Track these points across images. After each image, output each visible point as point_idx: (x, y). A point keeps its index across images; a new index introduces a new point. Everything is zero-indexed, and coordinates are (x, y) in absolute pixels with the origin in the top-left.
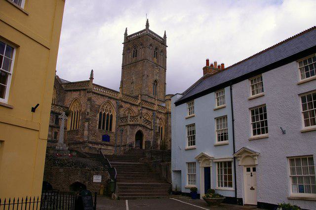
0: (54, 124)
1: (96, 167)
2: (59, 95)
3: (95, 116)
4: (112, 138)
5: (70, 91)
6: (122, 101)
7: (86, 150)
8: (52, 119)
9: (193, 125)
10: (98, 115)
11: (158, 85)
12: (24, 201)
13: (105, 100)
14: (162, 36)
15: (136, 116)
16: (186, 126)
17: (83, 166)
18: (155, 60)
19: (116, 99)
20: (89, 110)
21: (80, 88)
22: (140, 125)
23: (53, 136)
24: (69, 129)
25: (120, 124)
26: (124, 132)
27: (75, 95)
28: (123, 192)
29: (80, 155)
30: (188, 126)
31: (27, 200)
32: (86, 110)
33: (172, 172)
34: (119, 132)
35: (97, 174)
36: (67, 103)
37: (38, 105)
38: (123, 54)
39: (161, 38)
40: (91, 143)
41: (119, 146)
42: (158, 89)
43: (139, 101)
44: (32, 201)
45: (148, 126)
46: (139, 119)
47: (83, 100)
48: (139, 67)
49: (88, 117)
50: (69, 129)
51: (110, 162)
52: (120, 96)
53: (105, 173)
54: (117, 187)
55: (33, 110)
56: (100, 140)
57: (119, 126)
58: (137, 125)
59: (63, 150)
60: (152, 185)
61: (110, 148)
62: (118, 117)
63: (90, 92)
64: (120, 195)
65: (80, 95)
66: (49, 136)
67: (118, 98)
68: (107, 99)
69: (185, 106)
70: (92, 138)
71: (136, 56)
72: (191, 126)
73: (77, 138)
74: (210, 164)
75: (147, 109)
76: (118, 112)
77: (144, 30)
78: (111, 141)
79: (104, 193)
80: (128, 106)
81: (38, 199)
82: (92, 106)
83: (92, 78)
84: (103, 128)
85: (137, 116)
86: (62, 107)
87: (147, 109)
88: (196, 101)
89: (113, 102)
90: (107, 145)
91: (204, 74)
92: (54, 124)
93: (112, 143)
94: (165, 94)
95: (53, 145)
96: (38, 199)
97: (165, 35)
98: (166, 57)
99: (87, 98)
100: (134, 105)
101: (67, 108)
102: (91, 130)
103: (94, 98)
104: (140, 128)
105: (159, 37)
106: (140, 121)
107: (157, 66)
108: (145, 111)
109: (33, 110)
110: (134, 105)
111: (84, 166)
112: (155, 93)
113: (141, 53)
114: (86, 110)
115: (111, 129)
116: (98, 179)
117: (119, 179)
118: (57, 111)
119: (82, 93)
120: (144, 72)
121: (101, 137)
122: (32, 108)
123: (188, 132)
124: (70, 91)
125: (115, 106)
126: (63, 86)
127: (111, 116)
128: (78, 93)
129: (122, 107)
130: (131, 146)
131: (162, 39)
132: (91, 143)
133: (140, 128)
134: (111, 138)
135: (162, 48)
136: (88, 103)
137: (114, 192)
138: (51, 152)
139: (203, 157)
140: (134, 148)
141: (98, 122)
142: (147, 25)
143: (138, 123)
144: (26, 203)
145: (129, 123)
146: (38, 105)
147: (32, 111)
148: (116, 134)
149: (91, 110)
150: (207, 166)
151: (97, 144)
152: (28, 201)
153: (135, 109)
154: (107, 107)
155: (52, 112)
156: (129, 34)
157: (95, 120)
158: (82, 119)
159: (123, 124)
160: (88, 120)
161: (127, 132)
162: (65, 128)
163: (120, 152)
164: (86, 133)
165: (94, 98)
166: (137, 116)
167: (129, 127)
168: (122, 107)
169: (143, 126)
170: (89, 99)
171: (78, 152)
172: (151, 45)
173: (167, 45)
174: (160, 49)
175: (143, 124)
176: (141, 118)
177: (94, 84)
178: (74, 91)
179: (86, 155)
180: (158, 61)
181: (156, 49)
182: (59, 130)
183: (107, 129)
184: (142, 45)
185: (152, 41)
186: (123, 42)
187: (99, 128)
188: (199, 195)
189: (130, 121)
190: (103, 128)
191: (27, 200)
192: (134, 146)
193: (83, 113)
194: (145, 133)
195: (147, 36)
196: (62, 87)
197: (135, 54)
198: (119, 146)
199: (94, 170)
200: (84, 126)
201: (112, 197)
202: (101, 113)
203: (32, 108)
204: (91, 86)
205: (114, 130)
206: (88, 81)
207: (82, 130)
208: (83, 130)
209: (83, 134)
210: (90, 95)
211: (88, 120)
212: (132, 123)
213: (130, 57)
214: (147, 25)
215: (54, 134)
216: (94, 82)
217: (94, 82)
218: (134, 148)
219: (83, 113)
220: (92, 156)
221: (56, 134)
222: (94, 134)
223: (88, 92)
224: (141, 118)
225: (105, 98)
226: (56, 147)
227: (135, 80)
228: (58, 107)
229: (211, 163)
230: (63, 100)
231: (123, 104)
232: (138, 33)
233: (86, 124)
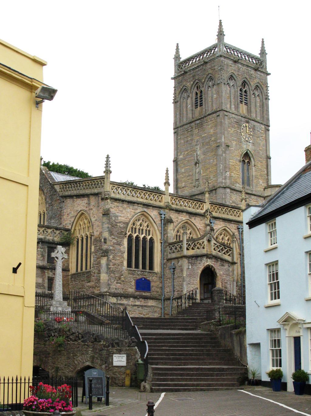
0: (45, 263)
1: (117, 341)
2: (51, 205)
3: (119, 244)
4: (155, 283)
5: (71, 197)
6: (171, 209)
7: (105, 310)
8: (40, 255)
9: (276, 263)
10: (125, 242)
11: (253, 163)
12: (14, 381)
13: (138, 211)
14: (256, 52)
15: (199, 239)
16: (266, 265)
17: (95, 339)
18: (243, 109)
19: (160, 208)
20: (106, 234)
21: (88, 191)
22: (208, 256)
23: (46, 285)
24: (73, 270)
25: (170, 256)
26: (177, 271)
27: (81, 204)
28: (158, 380)
29: (92, 319)
30: (269, 265)
31: (17, 380)
32: (101, 233)
33: (247, 346)
34: (168, 273)
35: (119, 352)
36: (67, 222)
37: (20, 264)
38: (175, 102)
39: (253, 57)
40: (115, 295)
41: (169, 299)
42: (254, 172)
43: (207, 206)
44: (23, 381)
45: (226, 257)
46: (206, 242)
47: (95, 215)
48: (209, 128)
49: (105, 247)
50: (73, 270)
51: (139, 331)
52: (166, 199)
53: (132, 350)
54: (150, 372)
55: (15, 270)
56: (131, 290)
57: (167, 261)
58: (202, 256)
59: (63, 313)
60: (219, 370)
61: (151, 303)
62: (166, 244)
63: (107, 199)
64: (154, 385)
65: (89, 204)
66: (38, 285)
67: (162, 204)
68: (140, 209)
69: (262, 228)
70: (116, 287)
71: (201, 105)
72: (273, 265)
73: (88, 287)
74: (299, 332)
75: (224, 220)
76: (164, 232)
77: (215, 47)
78: (153, 289)
79: (131, 383)
80: (184, 217)
81: (29, 380)
82: (113, 225)
83: (108, 172)
84: (137, 266)
85: (202, 237)
86: (57, 229)
87: (224, 220)
88: (280, 220)
89: (154, 213)
90: (146, 298)
91: (307, 160)
92: (45, 263)
93: (154, 294)
94: (268, 180)
95: (46, 301)
96: (29, 380)
97: (263, 52)
98: (267, 99)
99: (101, 211)
100: (196, 215)
101: (68, 230)
102: (113, 272)
103: (115, 209)
104: (209, 262)
105: (249, 55)
106: (210, 248)
107: (248, 122)
108: (218, 226)
109: (15, 270)
110: (196, 215)
111: (97, 339)
112: (247, 181)
113: (211, 94)
114: (101, 233)
115: (151, 267)
116: (120, 361)
117: (153, 359)
118: (50, 238)
119: (93, 200)
120: (221, 138)
121: (133, 283)
122: (14, 268)
123: (270, 276)
124: (71, 197)
125: (158, 220)
126: (57, 187)
127: (151, 240)
128: (86, 200)
129: (170, 221)
130: (191, 297)
131: (256, 59)
132: (115, 295)
133: (209, 262)
134: (152, 284)
135: (256, 81)
136: (105, 219)
137: (144, 380)
138: (36, 329)
139: (288, 320)
140: (198, 301)
141: (126, 255)
142: (221, 34)
143: (204, 251)
144: (17, 383)
145: (186, 252)
146: (20, 264)
147: (13, 272)
148: (162, 277)
149: (111, 233)
150: (297, 335)
151: (126, 296)
152: (19, 381)
153: (199, 223)
154: (141, 225)
155: (40, 242)
156: (184, 56)
157: (121, 251)
158: (95, 252)
159: (174, 256)
160: (106, 253)
161: (182, 271)
162: (65, 270)
163: (171, 309)
164: (104, 277)
165: (115, 209)
166: (202, 237)
167: (185, 261)
168: (170, 221)
169: (216, 258)
170: (106, 213)
171: (88, 315)
172: (231, 77)
173: (269, 70)
174: (253, 84)
175: (214, 253)
176: (209, 241)
177: (113, 183)
178: (79, 196)
179: (104, 319)
180: (249, 111)
181: (244, 83)
182: (54, 274)
183: (144, 267)
184: (211, 79)
185: (232, 68)
186: (173, 75)
187: (129, 265)
188: (285, 384)
189: (187, 249)
190: (137, 266)
191: (17, 380)
192: (198, 297)
193: (96, 240)
194: (220, 271)
195: (222, 59)
196: (56, 191)
197: (199, 101)
198: (169, 299)
199: (113, 346)
200: (99, 263)
201: (142, 388)
202: (130, 237)
203: (14, 268)
204: (108, 188)
205: (157, 268)
206: (102, 178)
207: (96, 271)
208: (99, 272)
209: (98, 280)
210: (109, 205)
211: (106, 253)
212: (191, 252)
213: (189, 106)
214: (221, 34)
215: (46, 281)
216: (114, 178)
217: (114, 178)
218: (198, 301)
219: (98, 240)
220: (114, 319)
221: (51, 281)
222: (120, 279)
223: (102, 199)
224: (209, 241)
225: (136, 206)
226: (52, 309)
227: (201, 158)
228: (49, 231)
229: (301, 331)
230: (59, 216)
231: (173, 216)
232: (202, 53)
233: (104, 261)
